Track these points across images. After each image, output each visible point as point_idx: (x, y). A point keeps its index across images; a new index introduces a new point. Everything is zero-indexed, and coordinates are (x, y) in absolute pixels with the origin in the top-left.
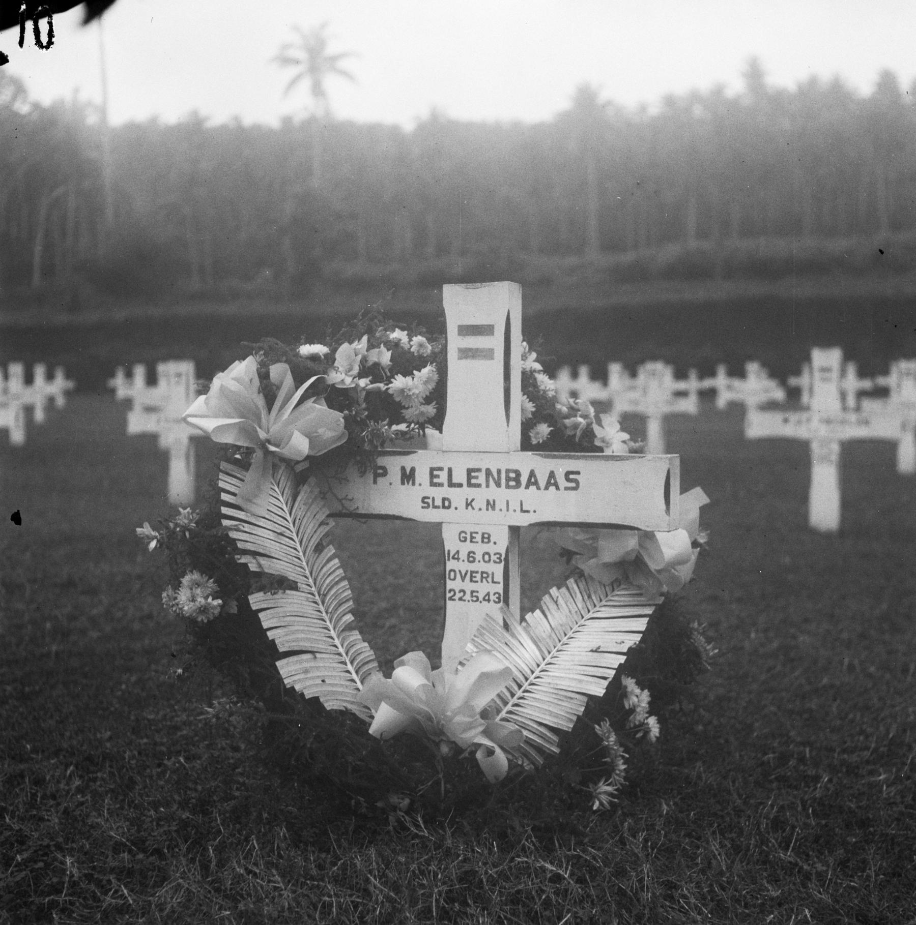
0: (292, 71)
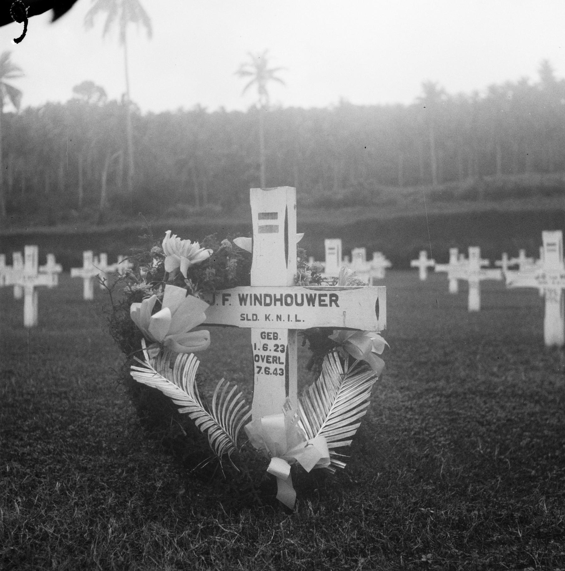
0: (247, 79)
